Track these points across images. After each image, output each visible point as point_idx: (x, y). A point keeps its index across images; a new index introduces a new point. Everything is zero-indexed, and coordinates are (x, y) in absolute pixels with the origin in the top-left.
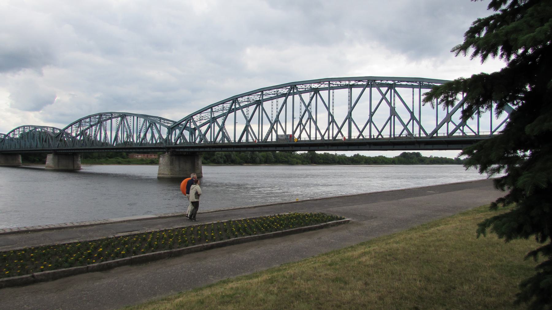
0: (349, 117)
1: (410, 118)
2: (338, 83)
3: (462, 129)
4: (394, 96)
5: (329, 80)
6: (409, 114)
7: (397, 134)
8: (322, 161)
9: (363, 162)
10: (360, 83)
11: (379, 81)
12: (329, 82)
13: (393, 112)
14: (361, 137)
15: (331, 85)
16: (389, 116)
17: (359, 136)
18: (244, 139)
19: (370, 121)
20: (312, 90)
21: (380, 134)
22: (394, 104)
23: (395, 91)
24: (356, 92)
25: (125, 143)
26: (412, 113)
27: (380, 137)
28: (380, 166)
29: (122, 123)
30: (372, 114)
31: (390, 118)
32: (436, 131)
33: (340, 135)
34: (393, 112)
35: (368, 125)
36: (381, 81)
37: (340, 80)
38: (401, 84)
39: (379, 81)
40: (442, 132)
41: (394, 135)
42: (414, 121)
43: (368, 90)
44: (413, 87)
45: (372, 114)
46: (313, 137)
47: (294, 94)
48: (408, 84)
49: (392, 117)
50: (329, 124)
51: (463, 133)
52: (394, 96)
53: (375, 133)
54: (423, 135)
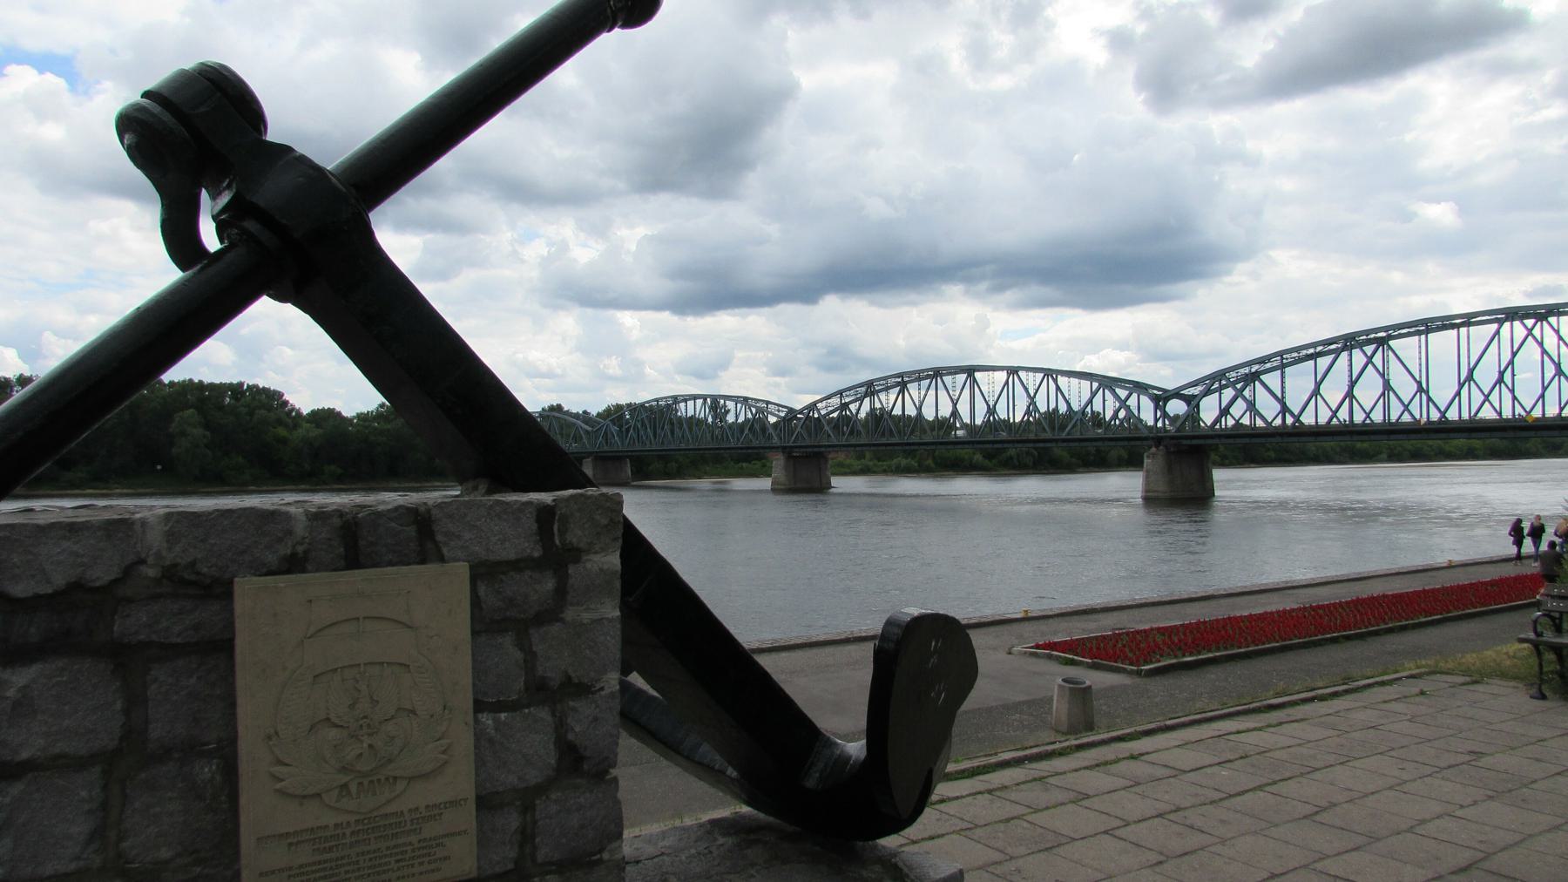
0: (1350, 395)
1: (1415, 389)
2: (1295, 355)
5: (1281, 354)
6: (1553, 367)
7: (1394, 418)
8: (1272, 454)
9: (1384, 456)
10: (1268, 365)
11: (1364, 337)
12: (1282, 356)
13: (1387, 386)
14: (1334, 421)
15: (1285, 361)
16: (1381, 390)
17: (1365, 420)
19: (1350, 395)
20: (1376, 340)
21: (1368, 416)
22: (1388, 374)
23: (1389, 346)
24: (1323, 362)
25: (1472, 420)
26: (1419, 383)
27: (1368, 421)
28: (1422, 466)
30: (1352, 384)
31: (1383, 394)
32: (1217, 420)
33: (1335, 419)
34: (1387, 386)
35: (1498, 386)
36: (1367, 335)
37: (1297, 349)
38: (1400, 334)
39: (1364, 337)
41: (1255, 424)
42: (1562, 377)
43: (1345, 355)
44: (1419, 333)
45: (1352, 384)
46: (1507, 414)
47: (1352, 347)
48: (1411, 330)
49: (1464, 392)
50: (1461, 386)
52: (1421, 377)
53: (1359, 417)
54: (1518, 410)
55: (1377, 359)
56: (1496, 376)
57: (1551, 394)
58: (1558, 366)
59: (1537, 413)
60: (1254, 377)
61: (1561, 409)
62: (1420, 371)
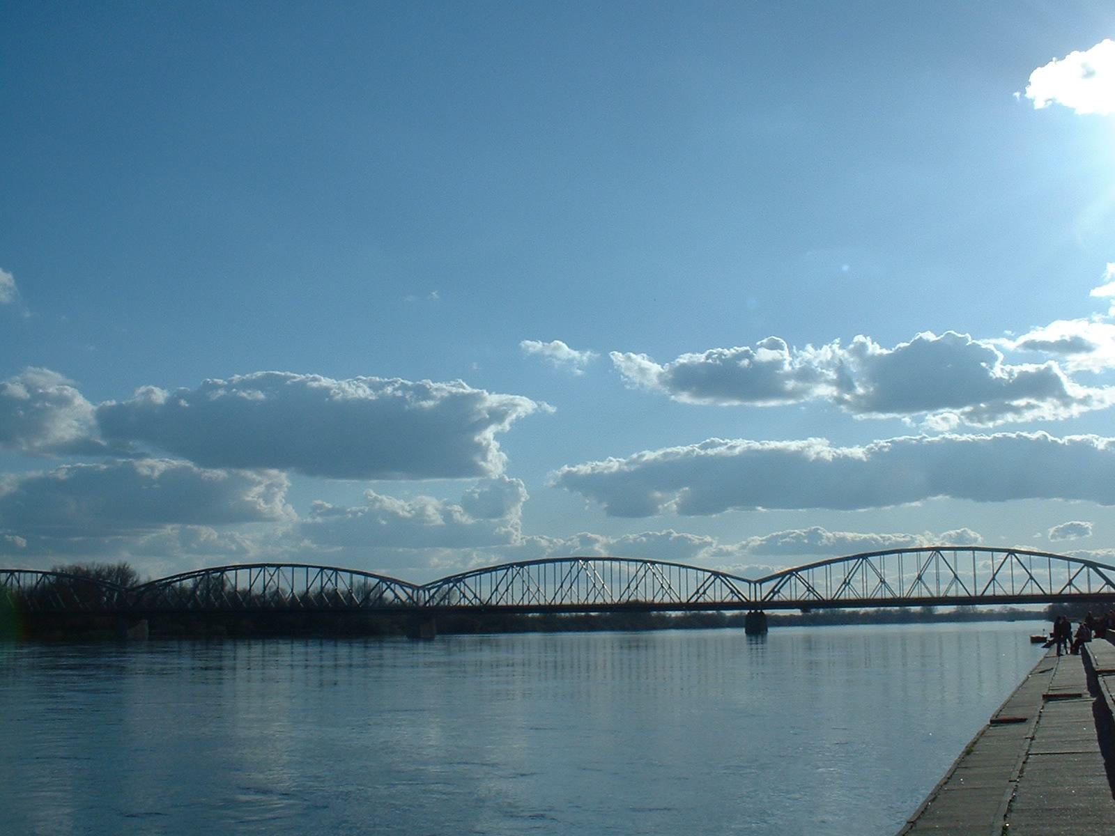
3: (393, 588)
4: (727, 580)
18: (693, 600)
29: (440, 587)
40: (625, 598)
51: (396, 596)
52: (727, 580)
54: (547, 603)
55: (275, 577)
56: (696, 590)
57: (526, 597)
58: (464, 594)
59: (553, 603)
60: (459, 580)
61: (629, 597)
62: (857, 569)
